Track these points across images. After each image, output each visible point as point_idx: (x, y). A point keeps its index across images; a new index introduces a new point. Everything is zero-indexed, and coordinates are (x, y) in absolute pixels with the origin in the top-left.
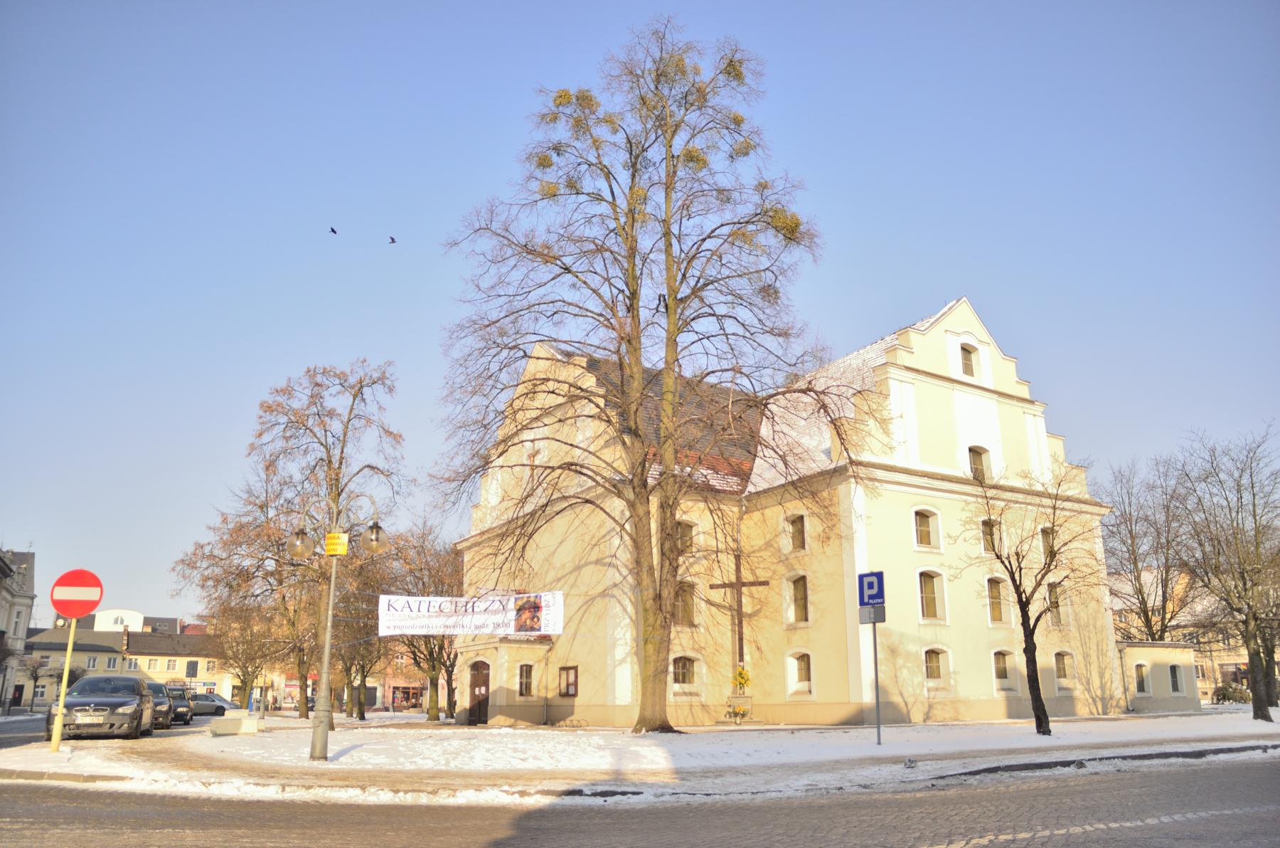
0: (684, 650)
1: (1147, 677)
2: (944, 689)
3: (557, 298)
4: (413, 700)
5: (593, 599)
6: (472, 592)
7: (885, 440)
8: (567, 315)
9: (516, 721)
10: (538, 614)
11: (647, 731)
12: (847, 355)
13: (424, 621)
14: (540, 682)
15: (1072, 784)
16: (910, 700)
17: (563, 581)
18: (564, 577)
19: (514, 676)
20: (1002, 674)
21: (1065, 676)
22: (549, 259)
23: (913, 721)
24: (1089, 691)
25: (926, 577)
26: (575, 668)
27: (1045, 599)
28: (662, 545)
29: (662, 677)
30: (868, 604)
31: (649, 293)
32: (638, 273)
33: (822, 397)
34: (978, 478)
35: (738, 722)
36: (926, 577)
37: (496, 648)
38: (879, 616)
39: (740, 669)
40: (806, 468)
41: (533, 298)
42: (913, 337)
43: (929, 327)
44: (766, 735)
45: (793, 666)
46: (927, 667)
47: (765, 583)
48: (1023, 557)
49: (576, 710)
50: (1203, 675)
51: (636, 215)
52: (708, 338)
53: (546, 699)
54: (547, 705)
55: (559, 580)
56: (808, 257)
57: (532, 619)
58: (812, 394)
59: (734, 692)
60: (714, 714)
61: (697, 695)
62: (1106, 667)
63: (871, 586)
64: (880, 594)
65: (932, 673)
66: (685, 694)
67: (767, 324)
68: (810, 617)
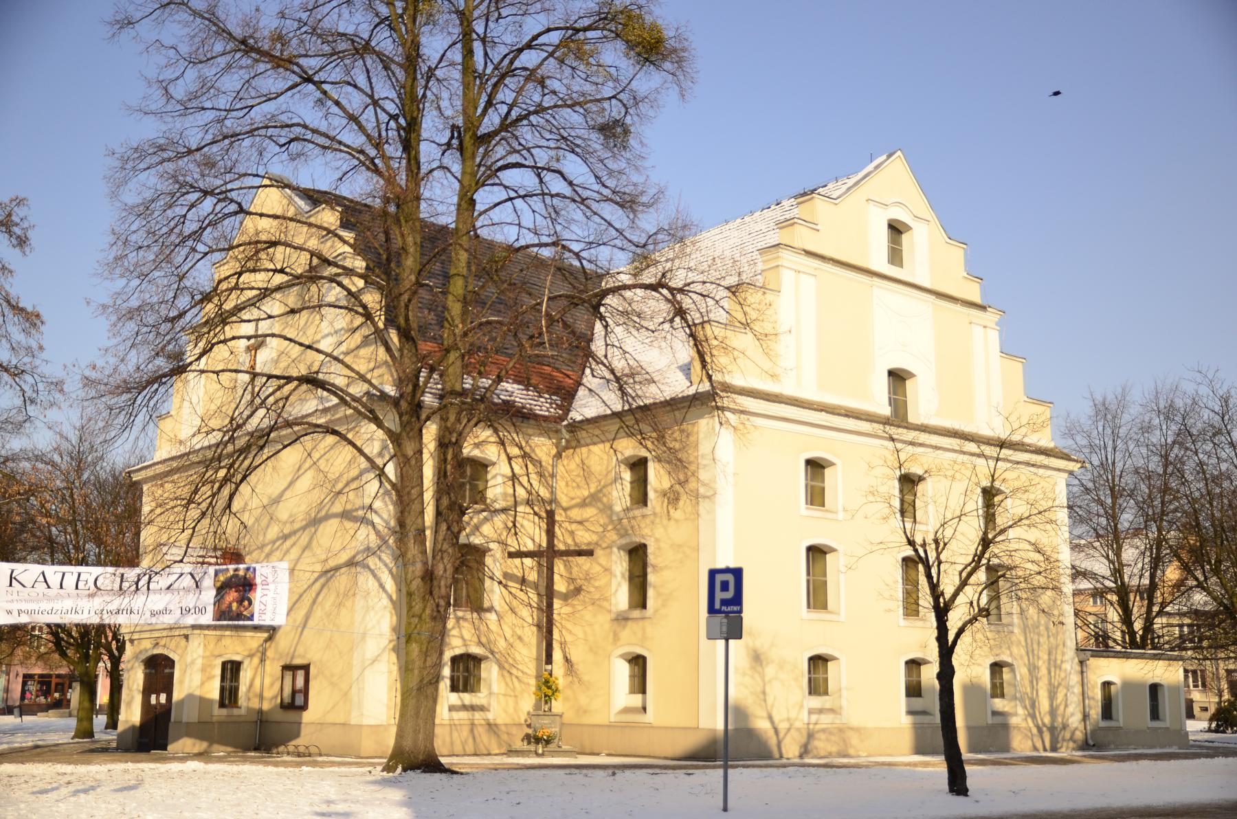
0: (465, 645)
1: (1117, 693)
2: (832, 711)
3: (295, 121)
4: (57, 695)
5: (337, 569)
6: (145, 562)
7: (767, 365)
8: (311, 146)
9: (211, 745)
10: (251, 595)
11: (405, 770)
12: (727, 222)
13: (68, 604)
14: (251, 685)
16: (783, 726)
17: (293, 539)
18: (294, 532)
19: (211, 678)
20: (914, 690)
21: (1002, 696)
22: (282, 63)
23: (785, 755)
24: (1033, 717)
25: (816, 553)
26: (306, 668)
27: (971, 603)
28: (437, 501)
29: (430, 690)
30: (719, 612)
31: (433, 129)
32: (420, 92)
33: (679, 297)
34: (898, 417)
35: (540, 751)
36: (816, 553)
37: (186, 637)
38: (734, 630)
39: (546, 674)
40: (652, 394)
41: (259, 114)
42: (819, 207)
43: (845, 193)
44: (579, 776)
45: (622, 672)
46: (810, 680)
47: (589, 553)
48: (945, 544)
49: (304, 731)
50: (1204, 685)
52: (523, 197)
53: (260, 712)
54: (261, 720)
55: (285, 537)
56: (672, 95)
57: (240, 602)
58: (665, 291)
59: (537, 706)
60: (505, 737)
61: (482, 708)
62: (1059, 684)
63: (725, 587)
64: (737, 600)
65: (817, 687)
66: (464, 707)
67: (608, 183)
68: (650, 602)
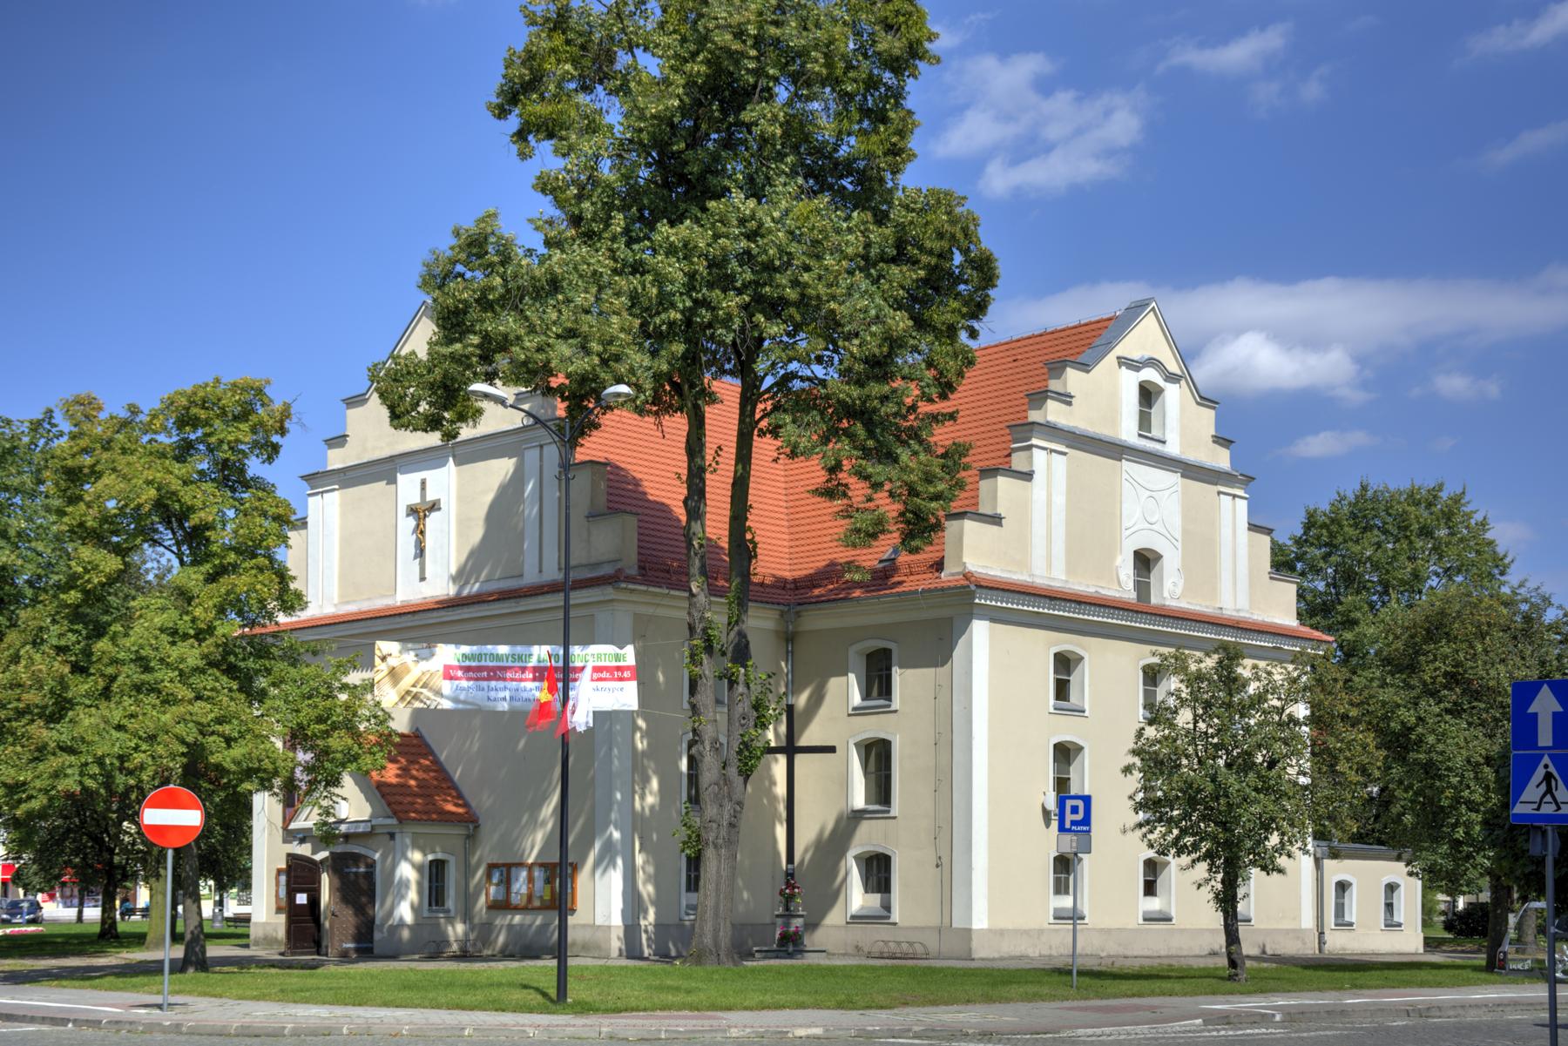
15: (419, 801)
30: (1069, 830)
51: (1506, 947)
63: (1075, 810)
64: (1086, 821)
